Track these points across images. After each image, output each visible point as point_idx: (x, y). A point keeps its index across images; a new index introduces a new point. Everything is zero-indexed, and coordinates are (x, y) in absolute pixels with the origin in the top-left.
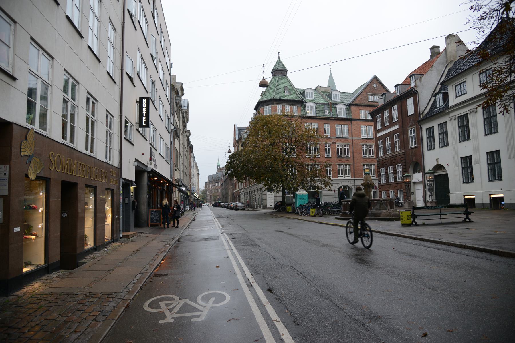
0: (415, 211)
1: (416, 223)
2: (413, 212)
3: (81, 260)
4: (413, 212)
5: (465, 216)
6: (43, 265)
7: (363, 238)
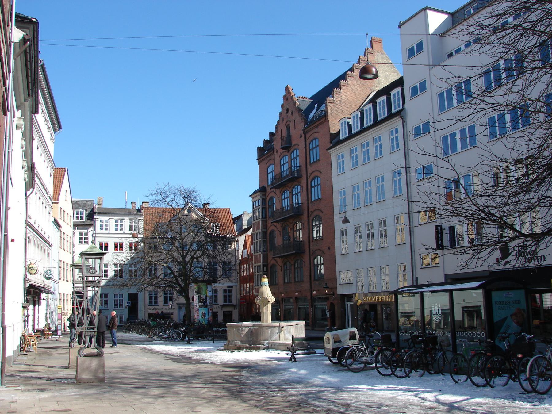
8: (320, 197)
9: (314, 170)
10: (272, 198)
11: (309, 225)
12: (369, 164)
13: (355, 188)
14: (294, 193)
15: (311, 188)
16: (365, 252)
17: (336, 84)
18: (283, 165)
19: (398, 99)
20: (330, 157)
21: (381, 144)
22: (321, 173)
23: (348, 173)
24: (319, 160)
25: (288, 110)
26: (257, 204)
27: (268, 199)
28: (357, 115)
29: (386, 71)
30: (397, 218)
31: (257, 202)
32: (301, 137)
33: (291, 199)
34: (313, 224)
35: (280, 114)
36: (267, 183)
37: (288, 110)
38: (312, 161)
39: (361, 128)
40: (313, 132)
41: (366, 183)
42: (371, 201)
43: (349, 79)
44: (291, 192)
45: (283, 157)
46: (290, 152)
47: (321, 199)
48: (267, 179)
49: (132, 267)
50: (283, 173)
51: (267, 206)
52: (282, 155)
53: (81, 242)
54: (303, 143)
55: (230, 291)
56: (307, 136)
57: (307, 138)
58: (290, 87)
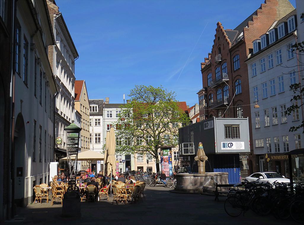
8: (241, 92)
9: (236, 75)
10: (210, 94)
11: (234, 110)
12: (265, 73)
13: (264, 84)
14: (224, 90)
15: (235, 86)
16: (271, 126)
17: (251, 18)
18: (209, 79)
19: (293, 23)
20: (246, 66)
21: (281, 55)
22: (241, 77)
23: (259, 76)
24: (239, 69)
25: (219, 38)
26: (202, 98)
27: (208, 95)
28: (264, 37)
29: (284, 7)
30: (265, 111)
31: (201, 97)
32: (228, 54)
33: (223, 94)
34: (237, 109)
35: (214, 41)
36: (207, 85)
37: (219, 38)
38: (235, 70)
39: (259, 50)
40: (236, 50)
41: (255, 88)
42: (275, 93)
43: (259, 14)
44: (223, 90)
45: (217, 68)
46: (221, 65)
47: (241, 93)
48: (207, 83)
49: (150, 139)
50: (217, 78)
51: (208, 99)
52: (216, 67)
53: (96, 125)
54: (230, 58)
55: (99, 135)
56: (232, 53)
57: (232, 55)
58: (220, 23)
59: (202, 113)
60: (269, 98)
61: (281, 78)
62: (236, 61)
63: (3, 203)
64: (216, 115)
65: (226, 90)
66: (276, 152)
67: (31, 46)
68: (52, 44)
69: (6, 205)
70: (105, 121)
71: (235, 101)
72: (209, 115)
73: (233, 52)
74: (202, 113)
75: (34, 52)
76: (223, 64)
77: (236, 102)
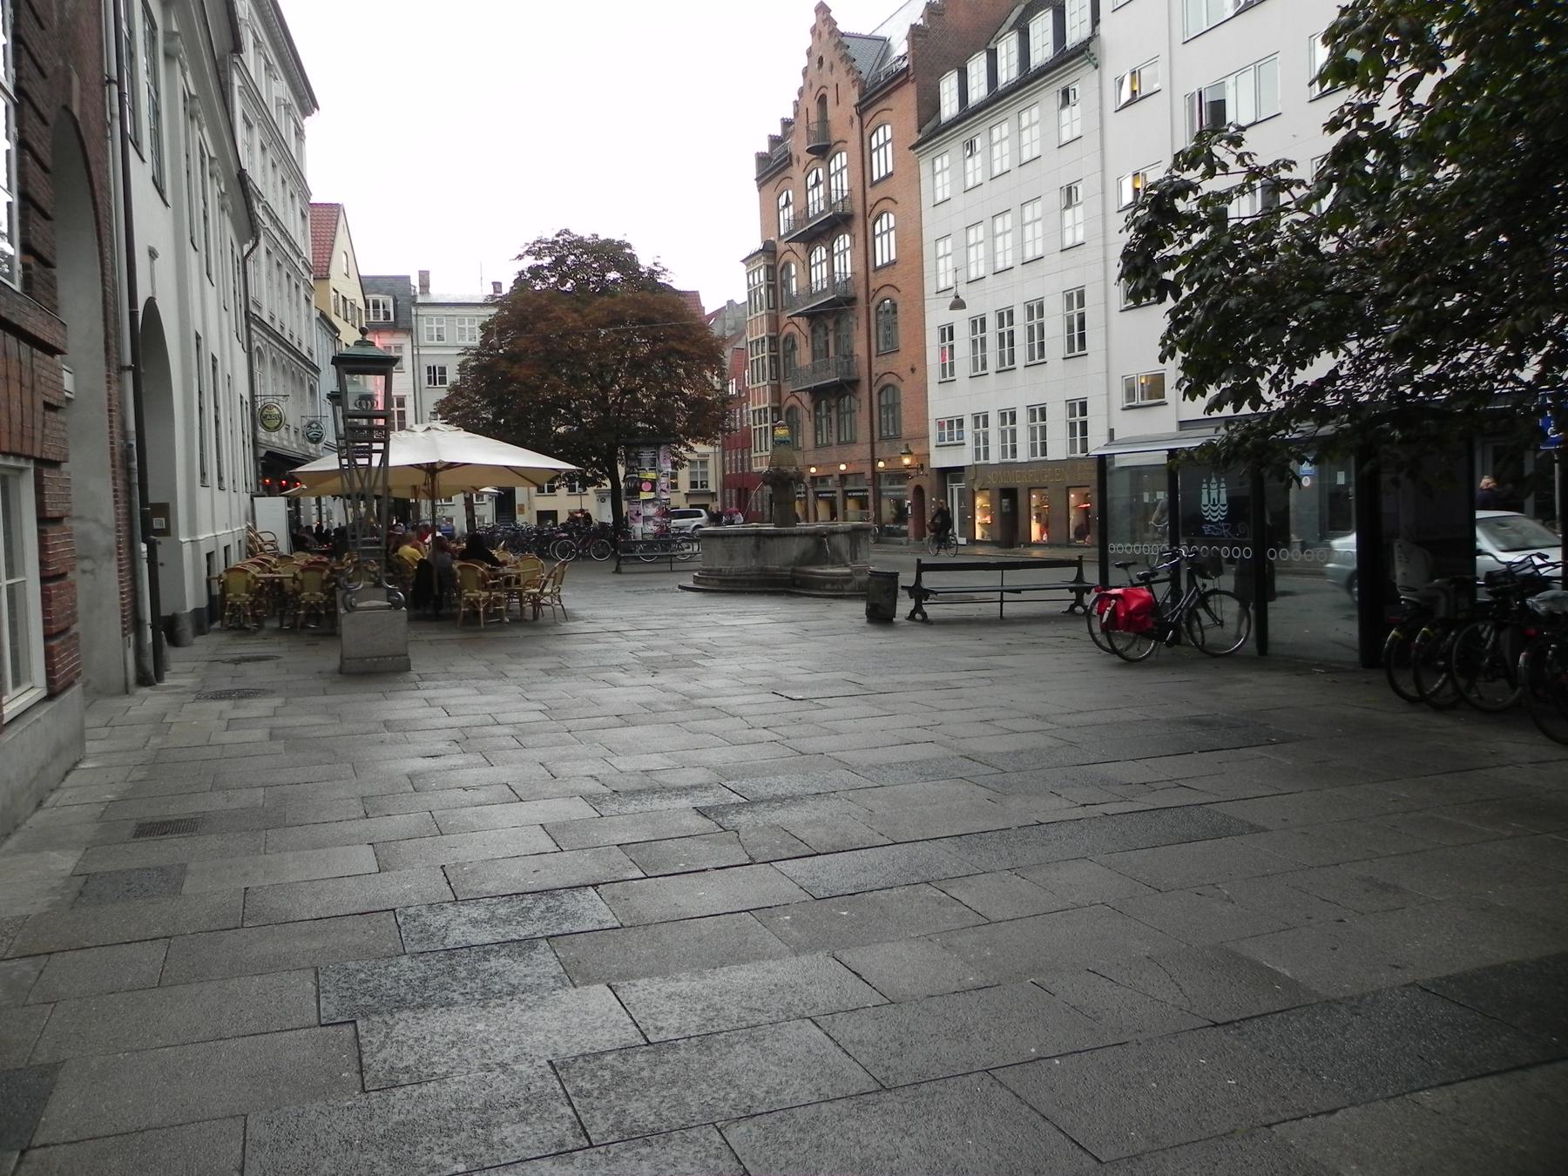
0: (924, 575)
1: (924, 615)
2: (919, 578)
3: (149, 673)
4: (919, 578)
5: (1073, 595)
6: (821, 213)
7: (1168, 583)
10: (787, 265)
14: (836, 251)
15: (871, 151)
35: (805, 72)
38: (876, 177)
44: (830, 251)
56: (867, 118)
59: (757, 331)
60: (990, 278)
61: (1008, 416)
62: (879, 147)
63: (124, 629)
64: (804, 262)
65: (842, 248)
66: (1005, 460)
67: (165, 41)
68: (443, 477)
69: (132, 636)
70: (417, 315)
71: (871, 289)
72: (782, 338)
73: (871, 113)
74: (757, 331)
75: (178, 65)
76: (834, 156)
77: (877, 291)
